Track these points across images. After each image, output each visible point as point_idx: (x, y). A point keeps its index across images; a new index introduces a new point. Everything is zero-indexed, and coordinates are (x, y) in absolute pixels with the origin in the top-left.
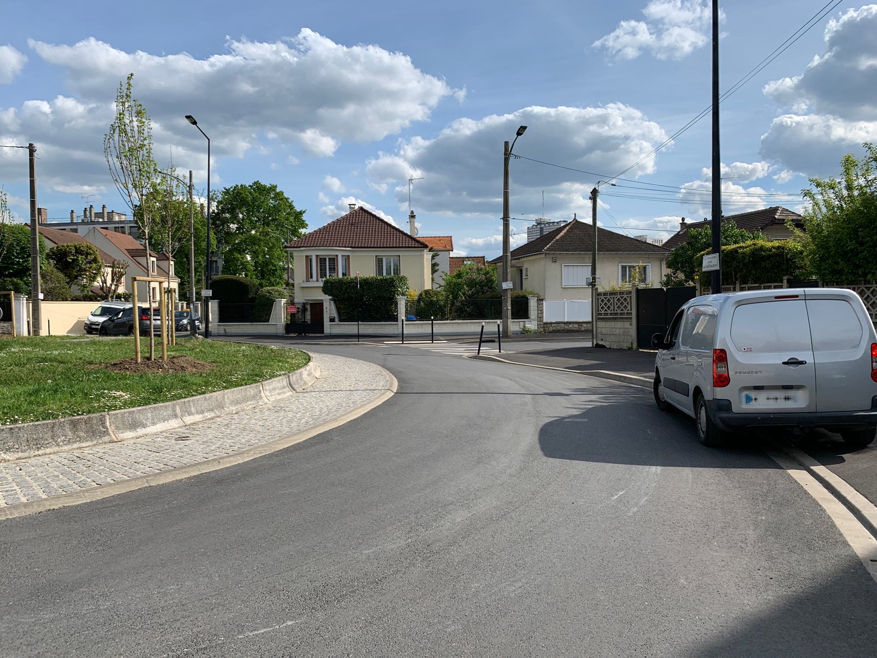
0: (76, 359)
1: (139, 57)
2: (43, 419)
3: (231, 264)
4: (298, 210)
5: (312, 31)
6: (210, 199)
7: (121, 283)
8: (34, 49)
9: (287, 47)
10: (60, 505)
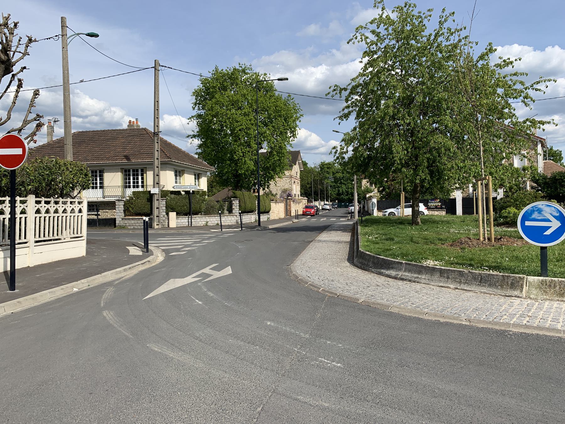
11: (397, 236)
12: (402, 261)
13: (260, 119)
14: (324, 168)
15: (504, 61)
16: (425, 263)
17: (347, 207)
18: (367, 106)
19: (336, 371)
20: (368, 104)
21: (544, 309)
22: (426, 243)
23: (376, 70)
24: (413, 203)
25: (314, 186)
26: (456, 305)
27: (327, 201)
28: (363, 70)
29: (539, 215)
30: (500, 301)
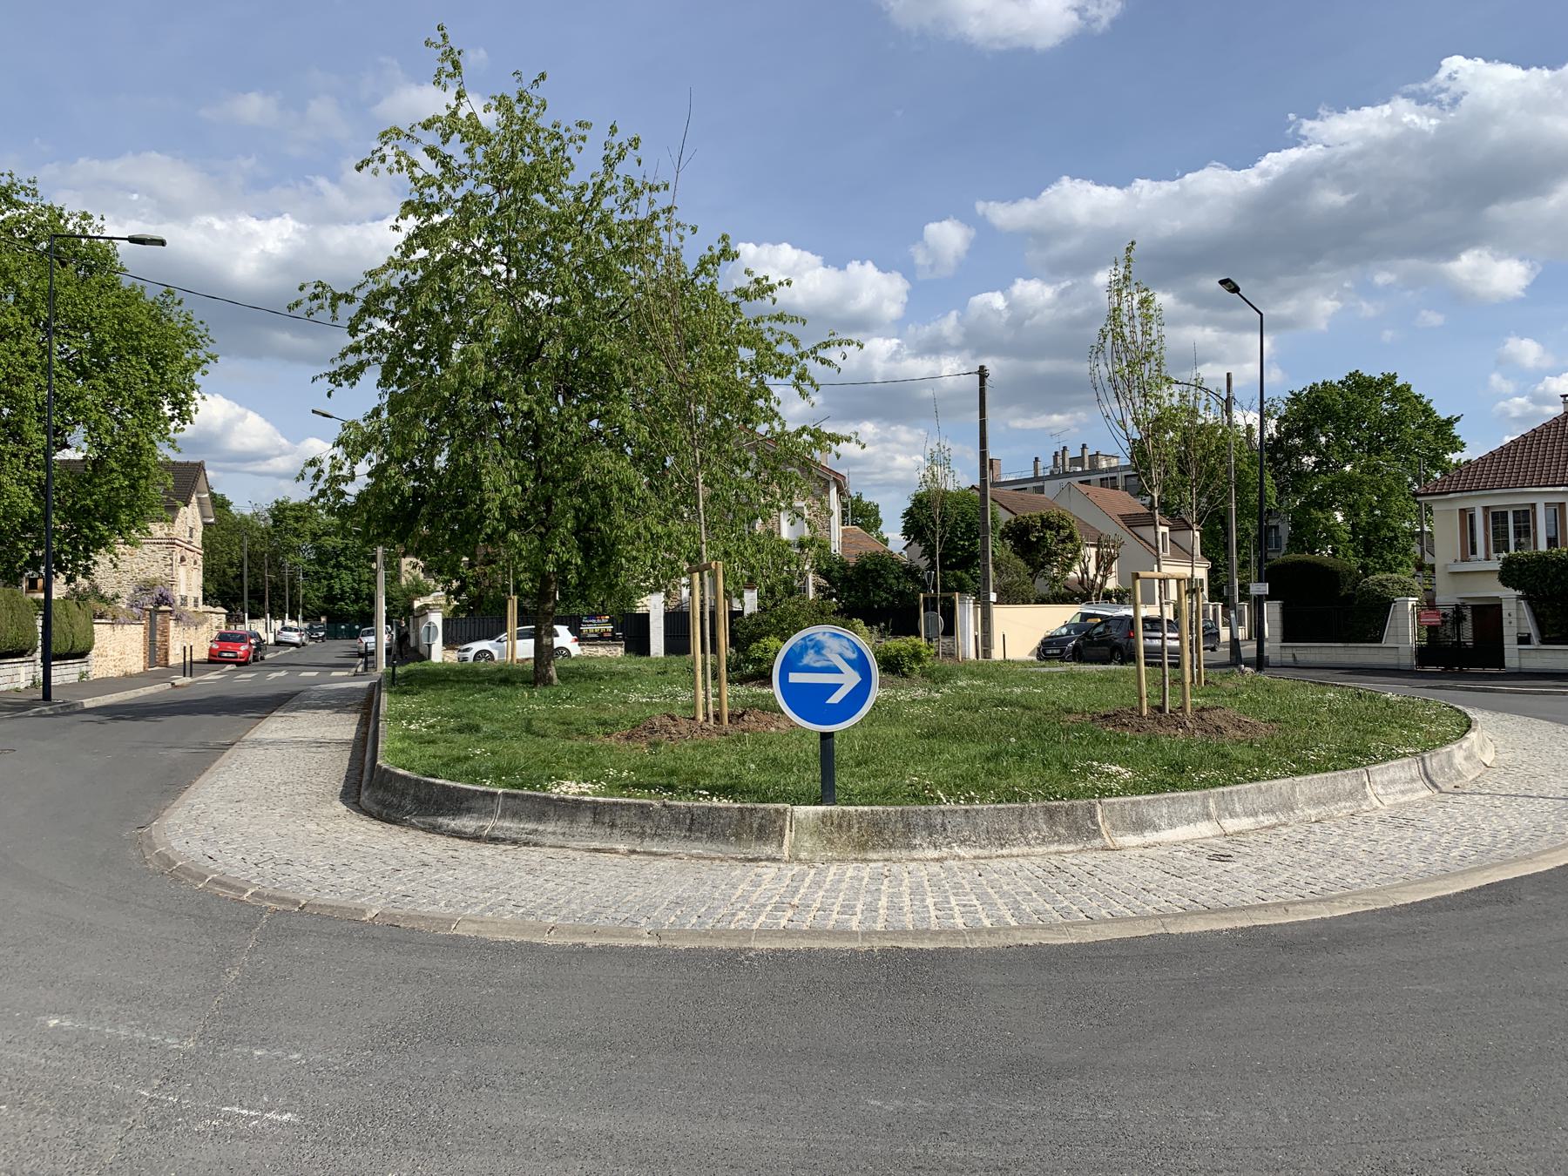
0: (1047, 704)
1: (1137, 189)
2: (1009, 801)
3: (1304, 534)
4: (1444, 417)
5: (1467, 57)
6: (1263, 415)
7: (1111, 573)
8: (984, 216)
9: (1413, 103)
10: (1036, 941)
11: (491, 720)
12: (495, 790)
13: (60, 353)
14: (285, 518)
15: (757, 281)
16: (558, 790)
17: (354, 635)
18: (414, 353)
19: (275, 1139)
20: (417, 347)
21: (827, 886)
22: (566, 735)
23: (438, 257)
24: (537, 622)
25: (249, 571)
26: (629, 898)
27: (293, 617)
28: (402, 253)
29: (817, 658)
30: (733, 874)
